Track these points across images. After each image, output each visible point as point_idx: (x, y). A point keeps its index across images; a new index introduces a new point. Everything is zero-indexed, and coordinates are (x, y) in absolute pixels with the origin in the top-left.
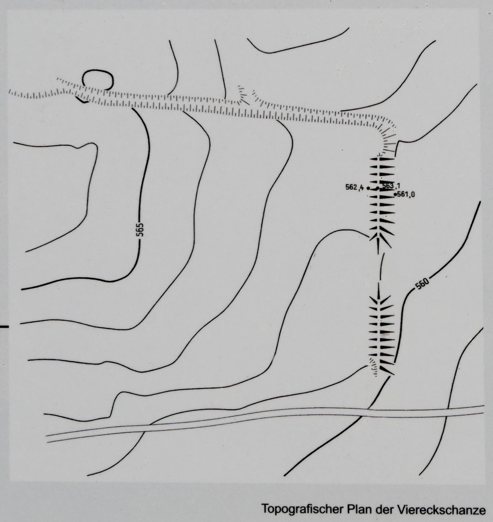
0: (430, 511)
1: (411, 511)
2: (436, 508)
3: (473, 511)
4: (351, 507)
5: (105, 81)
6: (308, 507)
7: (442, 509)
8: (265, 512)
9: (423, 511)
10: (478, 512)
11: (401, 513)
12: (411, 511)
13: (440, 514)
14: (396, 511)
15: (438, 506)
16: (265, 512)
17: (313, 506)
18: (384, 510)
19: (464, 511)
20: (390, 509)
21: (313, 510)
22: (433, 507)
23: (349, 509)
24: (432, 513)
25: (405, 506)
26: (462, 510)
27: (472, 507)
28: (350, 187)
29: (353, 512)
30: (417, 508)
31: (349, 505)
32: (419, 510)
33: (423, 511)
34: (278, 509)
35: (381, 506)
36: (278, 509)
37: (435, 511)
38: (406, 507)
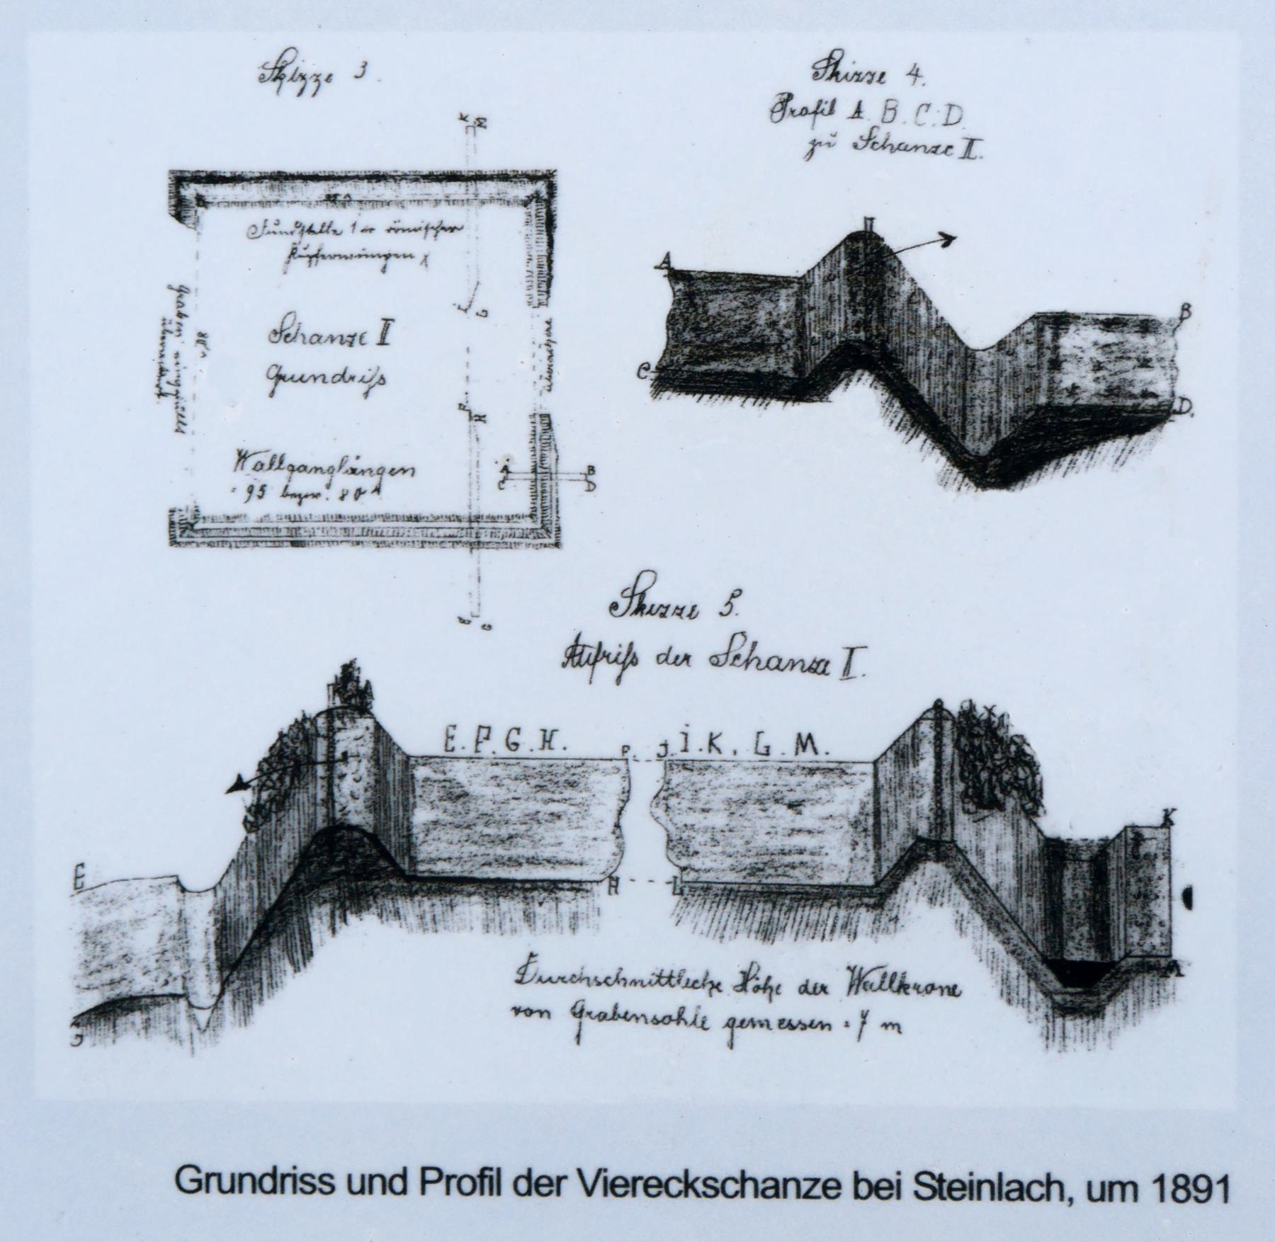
0: (675, 1187)
1: (615, 1186)
2: (691, 1179)
3: (805, 1186)
4: (432, 1175)
5: (514, 732)
6: (482, 1176)
7: (710, 1182)
8: (1162, 1199)
9: (656, 1186)
10: (818, 1191)
11: (589, 1193)
12: (615, 1186)
13: (704, 1198)
14: (572, 1187)
15: (699, 1171)
16: (1162, 1199)
17: (611, 1176)
18: (538, 1185)
19: (776, 1187)
20: (630, 1180)
21: (300, 1185)
22: (681, 1175)
23: (424, 1182)
24: (680, 1193)
25: (600, 1171)
26: (771, 1183)
27: (800, 1177)
28: (952, 991)
29: (437, 1190)
30: (635, 1180)
31: (424, 1169)
32: (640, 1184)
33: (656, 1186)
34: (268, 1184)
35: (530, 1170)
36: (268, 1184)
37: (689, 1186)
38: (603, 1175)
